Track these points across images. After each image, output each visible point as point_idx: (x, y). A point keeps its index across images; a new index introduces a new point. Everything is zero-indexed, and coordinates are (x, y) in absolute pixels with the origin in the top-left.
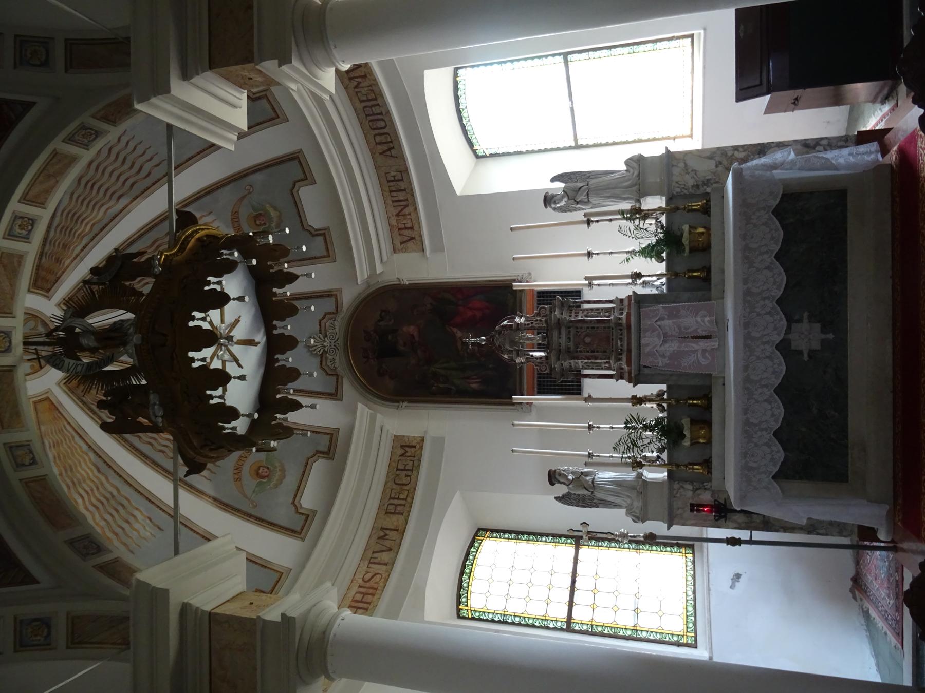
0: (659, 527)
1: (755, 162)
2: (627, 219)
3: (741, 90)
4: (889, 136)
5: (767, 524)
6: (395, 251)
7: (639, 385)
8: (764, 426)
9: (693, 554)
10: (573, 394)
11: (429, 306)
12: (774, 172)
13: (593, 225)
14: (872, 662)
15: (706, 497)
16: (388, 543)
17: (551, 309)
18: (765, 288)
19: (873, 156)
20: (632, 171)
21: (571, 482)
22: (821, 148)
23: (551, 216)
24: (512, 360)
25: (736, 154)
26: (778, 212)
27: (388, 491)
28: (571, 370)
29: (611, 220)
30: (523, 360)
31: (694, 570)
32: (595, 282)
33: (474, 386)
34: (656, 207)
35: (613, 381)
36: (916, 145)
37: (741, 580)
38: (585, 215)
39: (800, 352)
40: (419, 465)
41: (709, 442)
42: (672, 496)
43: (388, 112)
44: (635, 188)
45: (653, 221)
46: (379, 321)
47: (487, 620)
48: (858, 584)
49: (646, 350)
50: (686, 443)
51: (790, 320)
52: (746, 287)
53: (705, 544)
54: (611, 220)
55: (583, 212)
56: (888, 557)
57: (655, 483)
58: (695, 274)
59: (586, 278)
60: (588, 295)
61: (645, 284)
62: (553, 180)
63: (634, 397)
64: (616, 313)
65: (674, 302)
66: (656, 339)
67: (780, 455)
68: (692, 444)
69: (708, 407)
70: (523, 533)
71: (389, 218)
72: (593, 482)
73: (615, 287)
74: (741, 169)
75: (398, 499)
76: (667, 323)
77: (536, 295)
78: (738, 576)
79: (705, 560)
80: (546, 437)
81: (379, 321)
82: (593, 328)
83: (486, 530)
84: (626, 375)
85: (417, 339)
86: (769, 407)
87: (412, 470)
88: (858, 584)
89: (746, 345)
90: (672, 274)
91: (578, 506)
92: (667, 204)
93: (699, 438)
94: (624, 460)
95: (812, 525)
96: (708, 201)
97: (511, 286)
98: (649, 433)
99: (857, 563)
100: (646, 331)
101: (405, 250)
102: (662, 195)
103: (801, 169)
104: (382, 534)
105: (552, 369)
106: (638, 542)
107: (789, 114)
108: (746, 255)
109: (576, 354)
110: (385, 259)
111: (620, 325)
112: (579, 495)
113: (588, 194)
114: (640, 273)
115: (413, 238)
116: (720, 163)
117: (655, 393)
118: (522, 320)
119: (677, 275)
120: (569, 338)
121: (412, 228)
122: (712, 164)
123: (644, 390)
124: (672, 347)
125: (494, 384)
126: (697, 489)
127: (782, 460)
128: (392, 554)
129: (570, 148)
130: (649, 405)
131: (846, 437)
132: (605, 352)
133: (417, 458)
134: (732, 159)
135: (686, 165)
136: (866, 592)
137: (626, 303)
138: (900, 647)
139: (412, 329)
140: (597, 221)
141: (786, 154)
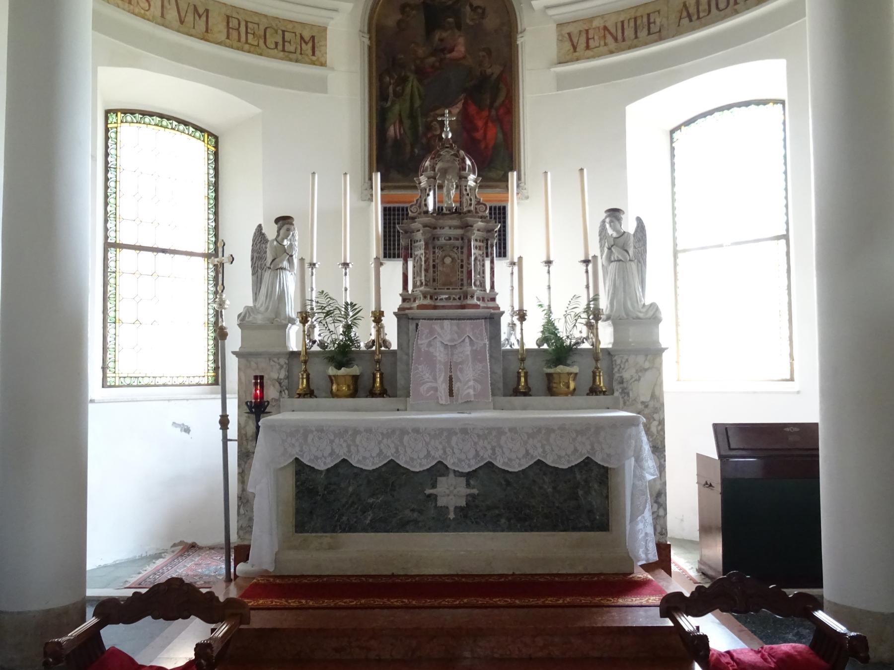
0: (234, 341)
1: (645, 439)
2: (588, 305)
3: (726, 429)
4: (663, 573)
5: (245, 456)
6: (560, 25)
7: (395, 319)
8: (353, 448)
9: (208, 385)
10: (385, 249)
11: (489, 71)
12: (633, 459)
13: (583, 267)
14: (109, 561)
15: (271, 393)
16: (190, 18)
17: (485, 217)
18: (504, 450)
19: (643, 556)
20: (644, 310)
21: (280, 244)
22: (655, 509)
23: (596, 216)
24: (425, 170)
25: (655, 423)
26: (588, 463)
27: (256, 19)
28: (413, 241)
29: (588, 287)
30: (423, 184)
31: (189, 385)
32: (516, 269)
33: (391, 131)
34: (600, 338)
35: (400, 290)
36: (653, 595)
37: (183, 433)
38: (595, 257)
39: (434, 486)
40: (291, 60)
41: (333, 395)
42: (272, 356)
43: (736, 12)
44: (624, 314)
45: (584, 335)
46: (471, 5)
47: (107, 147)
48: (192, 548)
49: (436, 325)
50: (332, 371)
51: (469, 476)
52: (507, 430)
53: (220, 396)
54: (588, 287)
55: (598, 254)
56: (219, 575)
57: (284, 338)
58: (523, 379)
59: (520, 258)
60: (501, 265)
61: (513, 326)
62: (639, 220)
63: (382, 314)
64: (478, 293)
65: (491, 356)
66: (449, 337)
67: (321, 466)
68: (330, 377)
69: (372, 394)
70: (216, 191)
71: (602, 16)
72: (282, 268)
73: (509, 292)
74: (638, 425)
75: (247, 33)
76: (468, 349)
77: (502, 204)
78: (187, 430)
79: (203, 396)
80: (331, 218)
81: (471, 5)
82: (462, 267)
83: (216, 146)
84: (407, 305)
85: (448, 56)
86: (374, 455)
87: (284, 50)
88: (192, 548)
89: (442, 431)
90: (523, 355)
91: (253, 251)
92: (603, 350)
93: (338, 385)
94: (308, 302)
95: (248, 501)
96: (604, 393)
97: (512, 170)
98: (341, 330)
99: (211, 548)
100: (458, 326)
101: (560, 40)
102: (614, 344)
103: (634, 486)
104: (201, 11)
105: (413, 219)
106: (216, 323)
107: (695, 479)
108: (544, 431)
109: (431, 246)
110: (551, 12)
111: (466, 297)
112: (266, 252)
113: (619, 261)
114: (525, 319)
115: (575, 48)
116: (646, 406)
117: (387, 338)
118: (471, 183)
119: (523, 360)
120: (450, 239)
121: (588, 47)
122: (645, 397)
123: (391, 325)
124: (440, 355)
125: (394, 154)
126: (280, 383)
127: (316, 467)
128: (177, 24)
129: (675, 245)
130: (373, 332)
131: (344, 531)
132: (434, 280)
133: (300, 57)
134: (650, 418)
135: (646, 370)
136: (181, 556)
137: (491, 304)
138: (127, 585)
139: (461, 49)
140: (587, 272)
141: (652, 471)
